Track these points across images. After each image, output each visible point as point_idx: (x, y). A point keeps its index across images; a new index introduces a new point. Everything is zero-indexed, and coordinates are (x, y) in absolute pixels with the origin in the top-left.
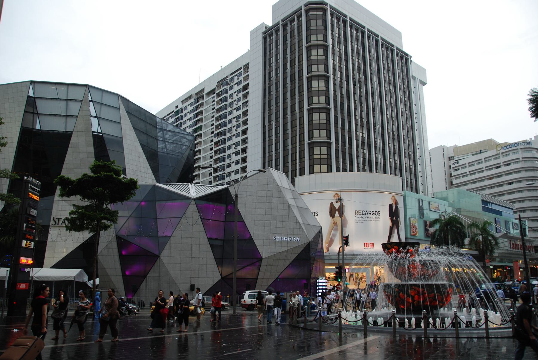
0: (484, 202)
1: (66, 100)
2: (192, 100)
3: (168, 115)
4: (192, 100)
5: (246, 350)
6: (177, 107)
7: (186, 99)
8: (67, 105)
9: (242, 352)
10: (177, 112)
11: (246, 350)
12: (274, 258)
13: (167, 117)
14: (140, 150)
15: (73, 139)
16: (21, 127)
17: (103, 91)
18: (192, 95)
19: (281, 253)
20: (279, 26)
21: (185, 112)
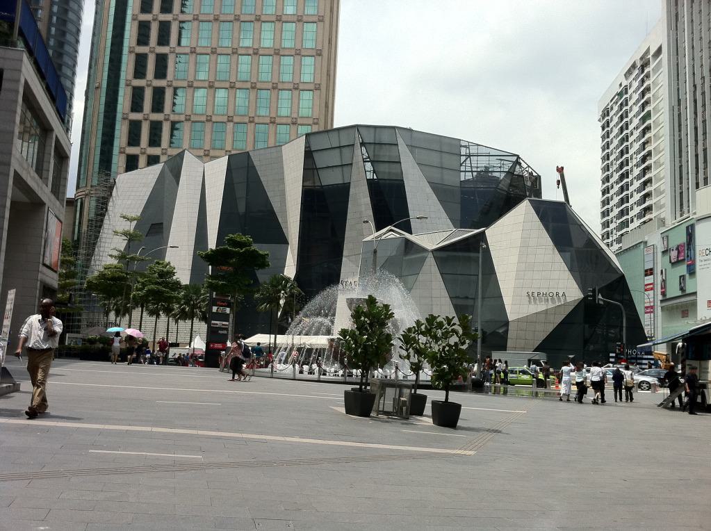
0: (683, 276)
1: (340, 147)
2: (636, 72)
3: (611, 101)
4: (636, 72)
5: (200, 432)
6: (621, 85)
7: (629, 70)
8: (341, 153)
9: (191, 435)
10: (620, 94)
11: (200, 432)
12: (528, 320)
13: (610, 105)
14: (429, 190)
15: (352, 191)
16: (303, 186)
17: (375, 127)
18: (635, 62)
19: (536, 313)
20: (45, 180)
21: (630, 91)
